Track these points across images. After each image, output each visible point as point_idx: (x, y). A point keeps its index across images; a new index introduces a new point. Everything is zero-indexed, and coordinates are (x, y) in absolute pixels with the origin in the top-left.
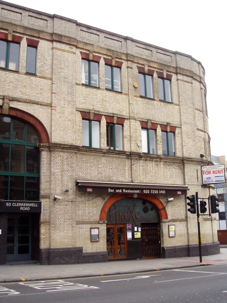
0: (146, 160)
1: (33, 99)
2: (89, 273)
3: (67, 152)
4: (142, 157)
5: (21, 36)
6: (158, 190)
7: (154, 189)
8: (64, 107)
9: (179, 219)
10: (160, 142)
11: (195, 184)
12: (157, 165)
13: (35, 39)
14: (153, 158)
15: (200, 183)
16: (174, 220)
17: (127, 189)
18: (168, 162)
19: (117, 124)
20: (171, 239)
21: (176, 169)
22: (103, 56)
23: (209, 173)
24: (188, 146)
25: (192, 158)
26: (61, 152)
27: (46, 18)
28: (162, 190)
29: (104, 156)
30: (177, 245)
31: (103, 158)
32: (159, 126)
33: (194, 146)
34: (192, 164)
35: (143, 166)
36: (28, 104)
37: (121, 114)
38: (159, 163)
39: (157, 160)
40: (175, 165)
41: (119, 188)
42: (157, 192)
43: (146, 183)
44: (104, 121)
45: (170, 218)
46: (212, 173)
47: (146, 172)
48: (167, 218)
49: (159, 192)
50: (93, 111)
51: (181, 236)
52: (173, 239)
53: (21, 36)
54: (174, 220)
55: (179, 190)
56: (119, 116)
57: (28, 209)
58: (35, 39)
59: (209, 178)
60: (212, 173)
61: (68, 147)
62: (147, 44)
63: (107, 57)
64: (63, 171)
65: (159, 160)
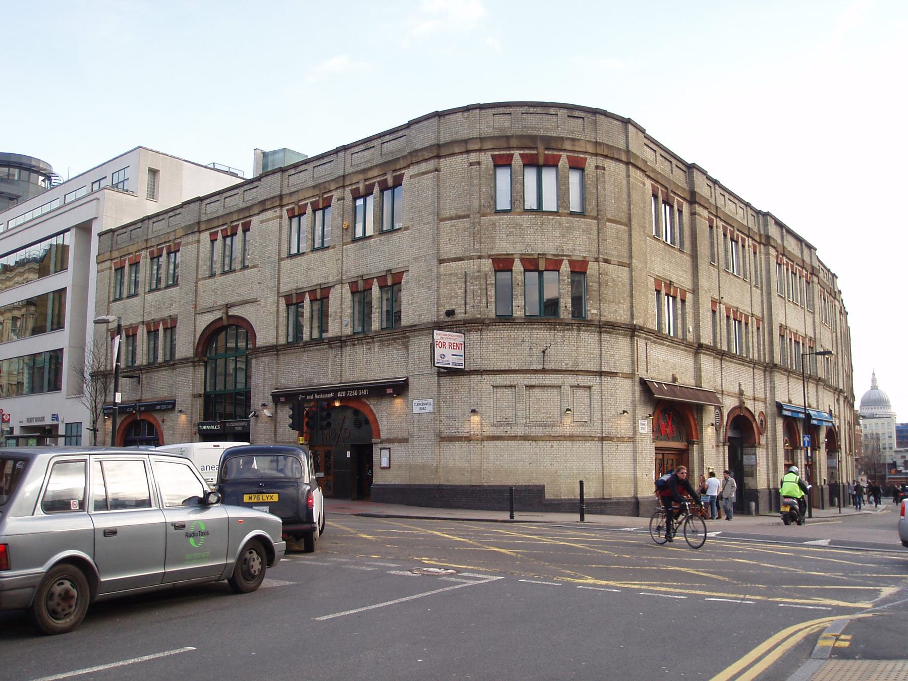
0: (354, 345)
1: (246, 298)
2: (748, 518)
3: (268, 355)
4: (345, 341)
5: (248, 219)
6: (358, 389)
7: (352, 389)
8: (267, 297)
9: (400, 437)
10: (376, 308)
11: (426, 372)
12: (370, 349)
13: (582, 156)
14: (362, 340)
15: (435, 370)
16: (389, 441)
17: (319, 393)
18: (387, 341)
19: (546, 270)
20: (384, 472)
21: (398, 350)
22: (565, 153)
23: (444, 345)
24: (417, 302)
25: (415, 326)
26: (263, 356)
27: (582, 114)
28: (364, 388)
29: (305, 351)
30: (392, 483)
31: (305, 354)
32: (375, 280)
33: (429, 298)
34: (422, 335)
35: (350, 355)
36: (242, 306)
37: (326, 281)
38: (372, 345)
39: (368, 340)
40: (398, 343)
41: (309, 393)
42: (355, 393)
43: (352, 382)
44: (565, 267)
45: (384, 435)
46: (447, 346)
47: (353, 364)
48: (379, 436)
49: (358, 393)
50: (294, 291)
51: (400, 467)
52: (387, 471)
53: (248, 219)
54: (389, 441)
55: (389, 387)
56: (322, 286)
57: (240, 429)
58: (582, 156)
59: (444, 355)
60: (447, 346)
61: (265, 349)
62: (365, 141)
63: (314, 199)
64: (265, 380)
65: (370, 340)
